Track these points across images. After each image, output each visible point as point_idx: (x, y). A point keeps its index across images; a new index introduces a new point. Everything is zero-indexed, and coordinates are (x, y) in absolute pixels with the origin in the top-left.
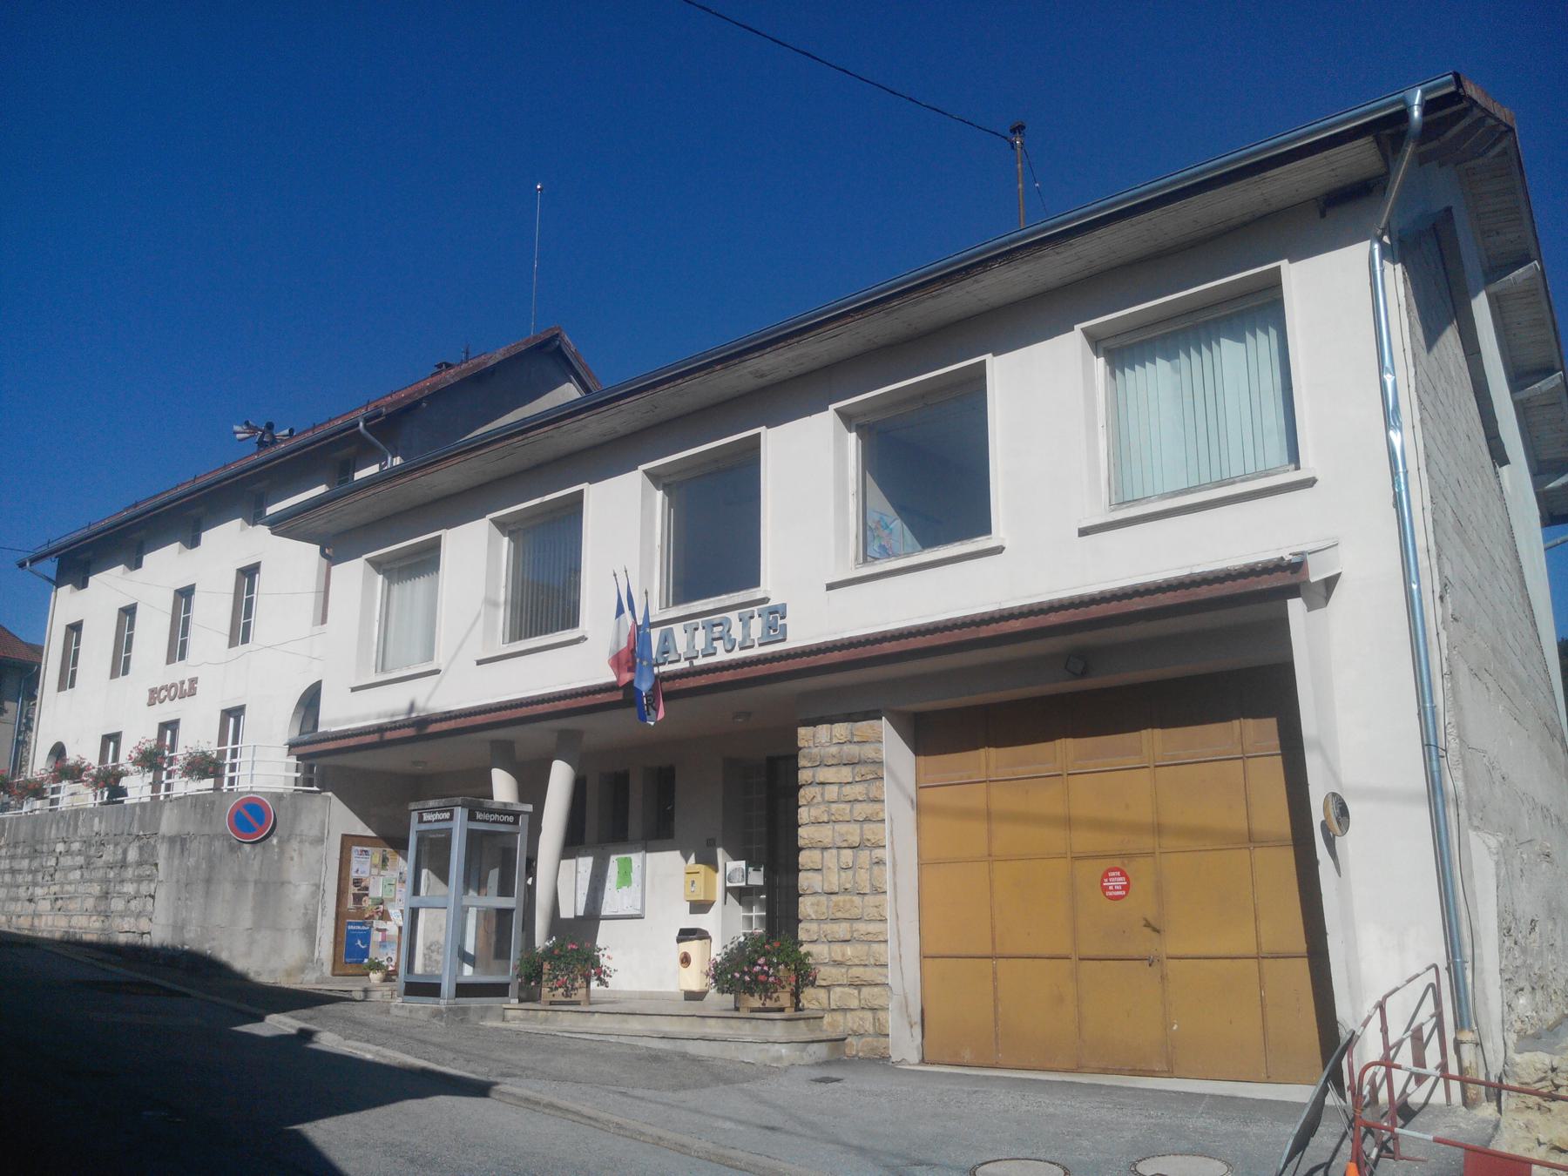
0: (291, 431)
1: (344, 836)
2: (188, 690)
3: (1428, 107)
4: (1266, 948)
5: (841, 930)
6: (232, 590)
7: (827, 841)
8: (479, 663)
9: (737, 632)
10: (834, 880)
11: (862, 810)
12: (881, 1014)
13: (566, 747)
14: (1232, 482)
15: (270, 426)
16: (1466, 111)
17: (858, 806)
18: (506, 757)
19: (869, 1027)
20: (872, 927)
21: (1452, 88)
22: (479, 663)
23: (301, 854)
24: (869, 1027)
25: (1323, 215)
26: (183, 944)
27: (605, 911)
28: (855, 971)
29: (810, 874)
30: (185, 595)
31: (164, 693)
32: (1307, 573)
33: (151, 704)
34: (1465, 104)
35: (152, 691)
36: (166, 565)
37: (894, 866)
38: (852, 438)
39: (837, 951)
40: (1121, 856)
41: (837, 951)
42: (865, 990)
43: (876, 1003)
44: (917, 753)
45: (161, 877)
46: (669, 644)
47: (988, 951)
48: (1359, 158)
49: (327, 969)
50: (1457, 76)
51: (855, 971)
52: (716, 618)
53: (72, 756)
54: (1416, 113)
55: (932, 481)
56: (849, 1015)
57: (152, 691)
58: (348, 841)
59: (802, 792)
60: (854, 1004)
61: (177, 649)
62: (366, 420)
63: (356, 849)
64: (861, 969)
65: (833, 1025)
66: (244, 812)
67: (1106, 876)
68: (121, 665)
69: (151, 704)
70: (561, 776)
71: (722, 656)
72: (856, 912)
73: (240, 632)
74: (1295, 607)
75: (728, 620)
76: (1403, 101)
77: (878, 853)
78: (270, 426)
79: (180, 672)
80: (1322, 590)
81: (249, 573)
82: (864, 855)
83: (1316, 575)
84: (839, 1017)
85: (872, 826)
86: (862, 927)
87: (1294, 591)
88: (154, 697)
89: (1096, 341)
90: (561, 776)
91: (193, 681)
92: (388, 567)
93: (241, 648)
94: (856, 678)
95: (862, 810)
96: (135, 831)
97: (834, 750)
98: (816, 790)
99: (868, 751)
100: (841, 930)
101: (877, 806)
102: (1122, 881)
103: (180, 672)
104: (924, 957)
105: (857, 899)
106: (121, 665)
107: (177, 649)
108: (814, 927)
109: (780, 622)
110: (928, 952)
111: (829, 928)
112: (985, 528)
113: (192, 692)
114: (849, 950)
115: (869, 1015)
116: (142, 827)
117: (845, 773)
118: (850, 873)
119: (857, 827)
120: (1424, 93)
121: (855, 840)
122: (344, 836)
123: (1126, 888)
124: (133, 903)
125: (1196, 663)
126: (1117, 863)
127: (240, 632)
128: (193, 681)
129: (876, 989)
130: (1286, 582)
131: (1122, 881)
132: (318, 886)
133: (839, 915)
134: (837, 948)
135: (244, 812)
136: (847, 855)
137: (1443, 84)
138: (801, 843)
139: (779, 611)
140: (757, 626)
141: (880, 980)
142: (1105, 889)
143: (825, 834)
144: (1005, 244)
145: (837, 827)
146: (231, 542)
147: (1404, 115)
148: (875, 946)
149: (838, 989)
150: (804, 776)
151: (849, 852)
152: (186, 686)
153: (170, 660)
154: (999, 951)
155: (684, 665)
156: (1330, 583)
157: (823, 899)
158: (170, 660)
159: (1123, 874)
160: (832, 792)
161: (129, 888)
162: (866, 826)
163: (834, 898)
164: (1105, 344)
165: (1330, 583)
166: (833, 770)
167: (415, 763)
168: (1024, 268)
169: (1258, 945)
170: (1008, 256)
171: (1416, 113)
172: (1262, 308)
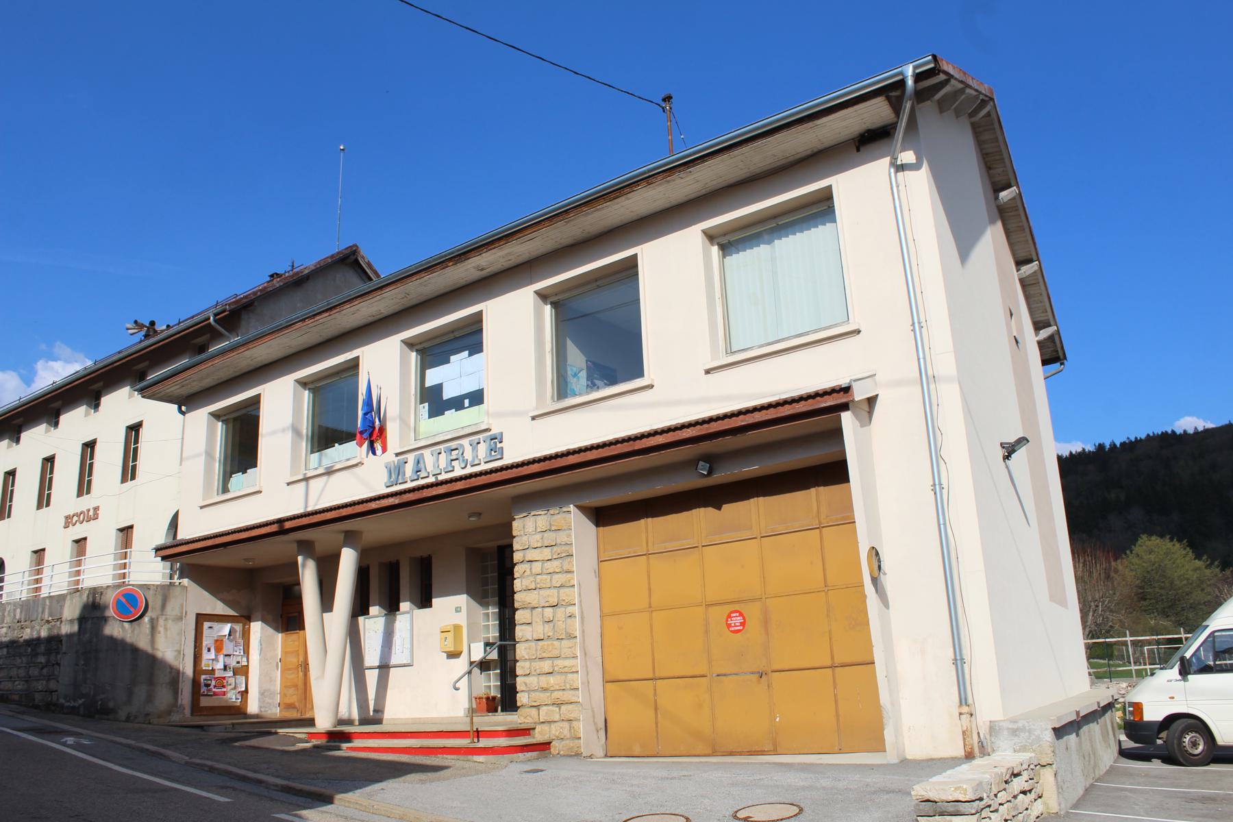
0: (168, 326)
1: (198, 615)
2: (92, 515)
3: (918, 77)
4: (837, 661)
5: (546, 666)
6: (123, 440)
7: (534, 604)
8: (288, 484)
9: (468, 455)
10: (539, 630)
11: (558, 579)
12: (574, 723)
13: (350, 538)
14: (807, 334)
15: (153, 323)
16: (946, 82)
17: (556, 577)
18: (306, 548)
19: (566, 732)
20: (567, 663)
21: (932, 65)
22: (288, 484)
23: (166, 629)
24: (566, 732)
25: (858, 150)
26: (1078, 713)
27: (393, 661)
28: (556, 694)
29: (524, 627)
30: (89, 447)
31: (75, 518)
32: (852, 395)
33: (66, 527)
34: (942, 77)
35: (67, 517)
36: (77, 423)
37: (582, 618)
38: (548, 309)
39: (544, 681)
40: (738, 602)
41: (544, 681)
42: (563, 707)
43: (571, 716)
44: (597, 525)
45: (64, 649)
46: (421, 465)
47: (651, 676)
48: (876, 112)
49: (188, 711)
50: (934, 57)
51: (556, 694)
52: (453, 444)
53: (495, 693)
54: (910, 82)
55: (602, 338)
56: (553, 726)
57: (67, 517)
58: (201, 618)
59: (516, 569)
60: (557, 718)
61: (84, 486)
62: (216, 315)
63: (206, 625)
64: (561, 693)
65: (540, 733)
66: (123, 600)
67: (729, 616)
68: (44, 499)
69: (66, 527)
70: (348, 560)
71: (459, 472)
72: (556, 653)
73: (129, 472)
74: (846, 418)
75: (462, 446)
76: (901, 73)
77: (570, 609)
78: (153, 323)
79: (86, 503)
80: (866, 407)
81: (134, 430)
82: (560, 612)
83: (859, 394)
84: (545, 727)
85: (566, 590)
86: (559, 662)
87: (845, 407)
88: (69, 521)
89: (710, 236)
90: (348, 560)
91: (96, 509)
92: (312, 386)
93: (130, 483)
94: (549, 480)
95: (558, 579)
96: (46, 617)
97: (538, 536)
98: (525, 566)
99: (562, 537)
100: (546, 666)
101: (569, 575)
102: (740, 619)
103: (86, 503)
104: (606, 682)
105: (556, 643)
106: (44, 499)
107: (84, 486)
108: (527, 664)
109: (499, 445)
110: (609, 678)
111: (538, 665)
112: (640, 373)
113: (96, 517)
114: (552, 680)
115: (566, 725)
116: (50, 615)
117: (547, 553)
118: (551, 624)
119: (555, 591)
120: (915, 68)
121: (554, 601)
122: (198, 615)
123: (743, 624)
124: (45, 671)
125: (787, 452)
126: (737, 607)
127: (129, 472)
128: (96, 509)
129: (570, 707)
130: (839, 402)
131: (740, 619)
132: (179, 652)
133: (544, 655)
134: (543, 678)
135: (123, 600)
136: (549, 612)
137: (926, 62)
138: (516, 605)
139: (497, 439)
140: (483, 449)
141: (574, 699)
142: (729, 626)
143: (531, 555)
144: (644, 173)
145: (542, 592)
146: (123, 404)
147: (901, 83)
148: (570, 676)
149: (545, 708)
150: (517, 557)
151: (550, 609)
152: (91, 513)
153: (80, 494)
154: (657, 675)
155: (432, 480)
156: (871, 401)
157: (533, 644)
158: (80, 494)
159: (741, 615)
160: (537, 567)
161: (42, 659)
162: (562, 590)
163: (540, 643)
164: (717, 241)
165: (871, 401)
166: (538, 551)
167: (246, 560)
168: (660, 189)
169: (832, 658)
170: (648, 179)
171: (910, 82)
172: (821, 208)
